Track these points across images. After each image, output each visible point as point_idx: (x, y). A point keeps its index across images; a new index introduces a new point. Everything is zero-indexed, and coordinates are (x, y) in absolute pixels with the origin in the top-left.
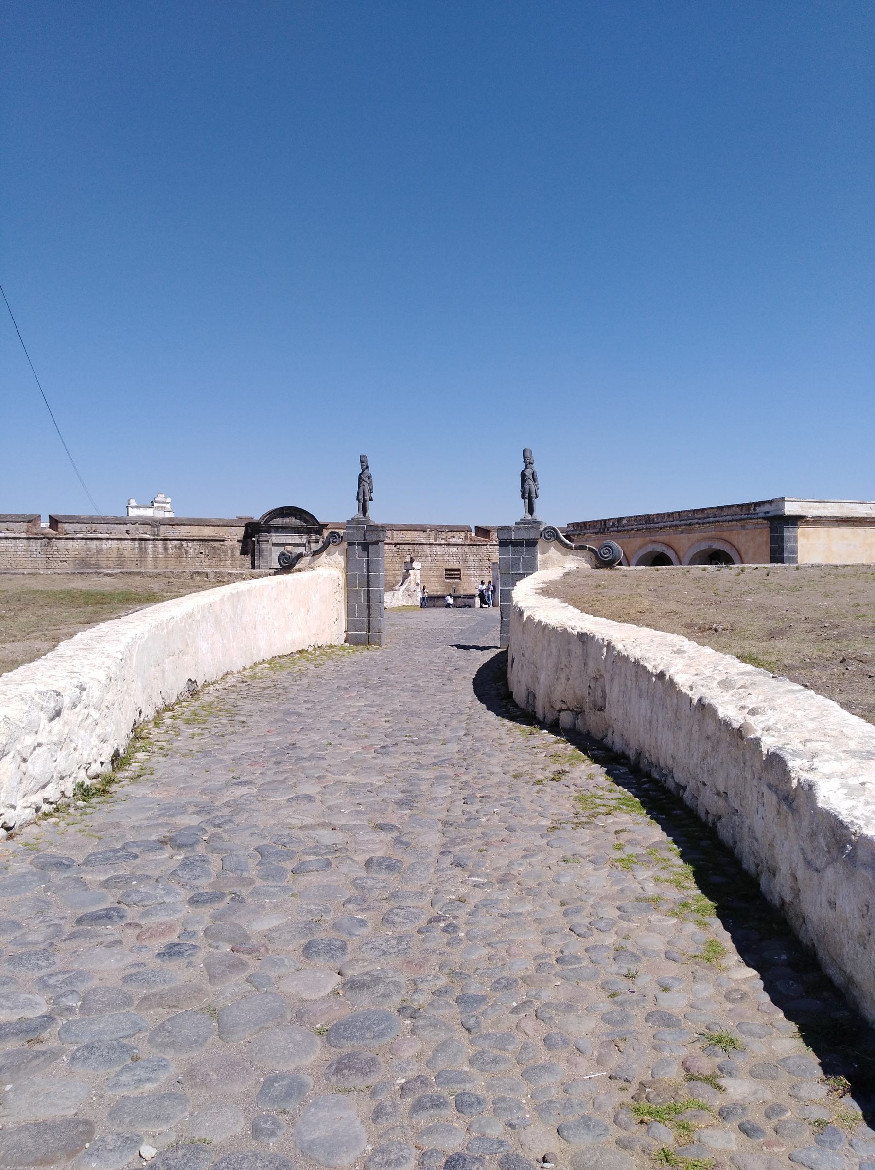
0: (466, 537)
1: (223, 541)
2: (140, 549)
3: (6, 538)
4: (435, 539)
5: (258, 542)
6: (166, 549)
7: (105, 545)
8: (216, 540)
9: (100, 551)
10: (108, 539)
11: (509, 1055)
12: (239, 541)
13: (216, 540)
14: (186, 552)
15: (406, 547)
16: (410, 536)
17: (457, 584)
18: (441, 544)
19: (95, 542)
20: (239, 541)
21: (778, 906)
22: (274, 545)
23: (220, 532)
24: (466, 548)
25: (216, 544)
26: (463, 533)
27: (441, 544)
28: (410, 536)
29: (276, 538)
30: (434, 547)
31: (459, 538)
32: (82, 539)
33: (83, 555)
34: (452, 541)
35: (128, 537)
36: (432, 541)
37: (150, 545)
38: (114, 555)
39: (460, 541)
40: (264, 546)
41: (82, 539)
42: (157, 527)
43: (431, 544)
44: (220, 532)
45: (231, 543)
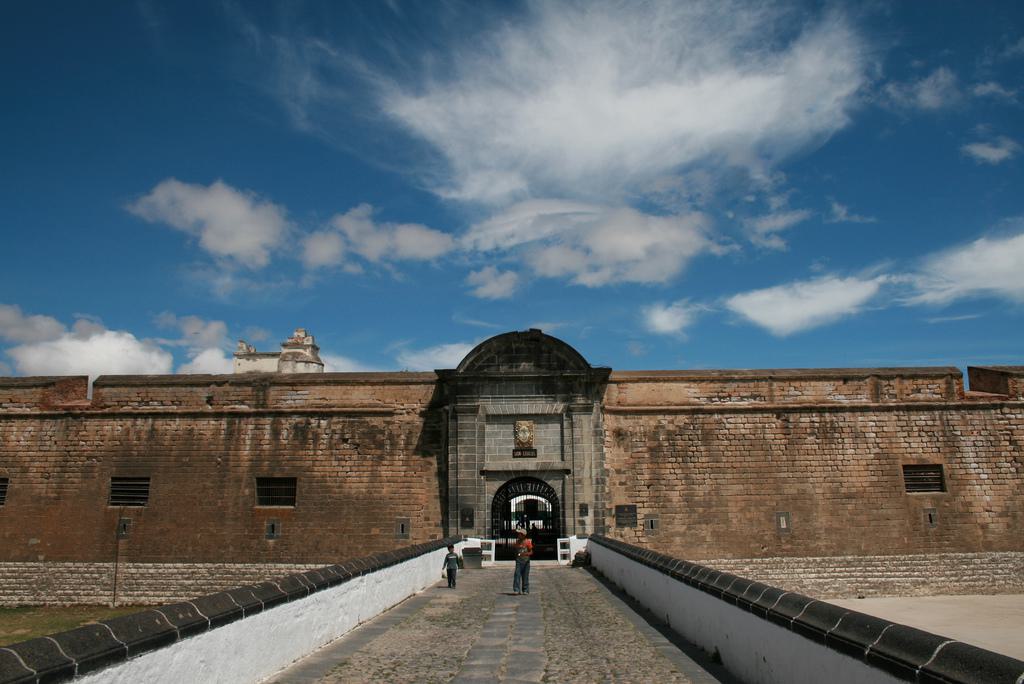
0: (949, 392)
1: (390, 414)
5: (455, 411)
6: (276, 433)
8: (376, 414)
11: (678, 548)
13: (376, 414)
21: (419, 112)
22: (494, 419)
23: (387, 397)
25: (376, 421)
28: (811, 393)
29: (89, 404)
31: (930, 392)
37: (249, 427)
40: (463, 421)
44: (387, 397)
45: (407, 418)
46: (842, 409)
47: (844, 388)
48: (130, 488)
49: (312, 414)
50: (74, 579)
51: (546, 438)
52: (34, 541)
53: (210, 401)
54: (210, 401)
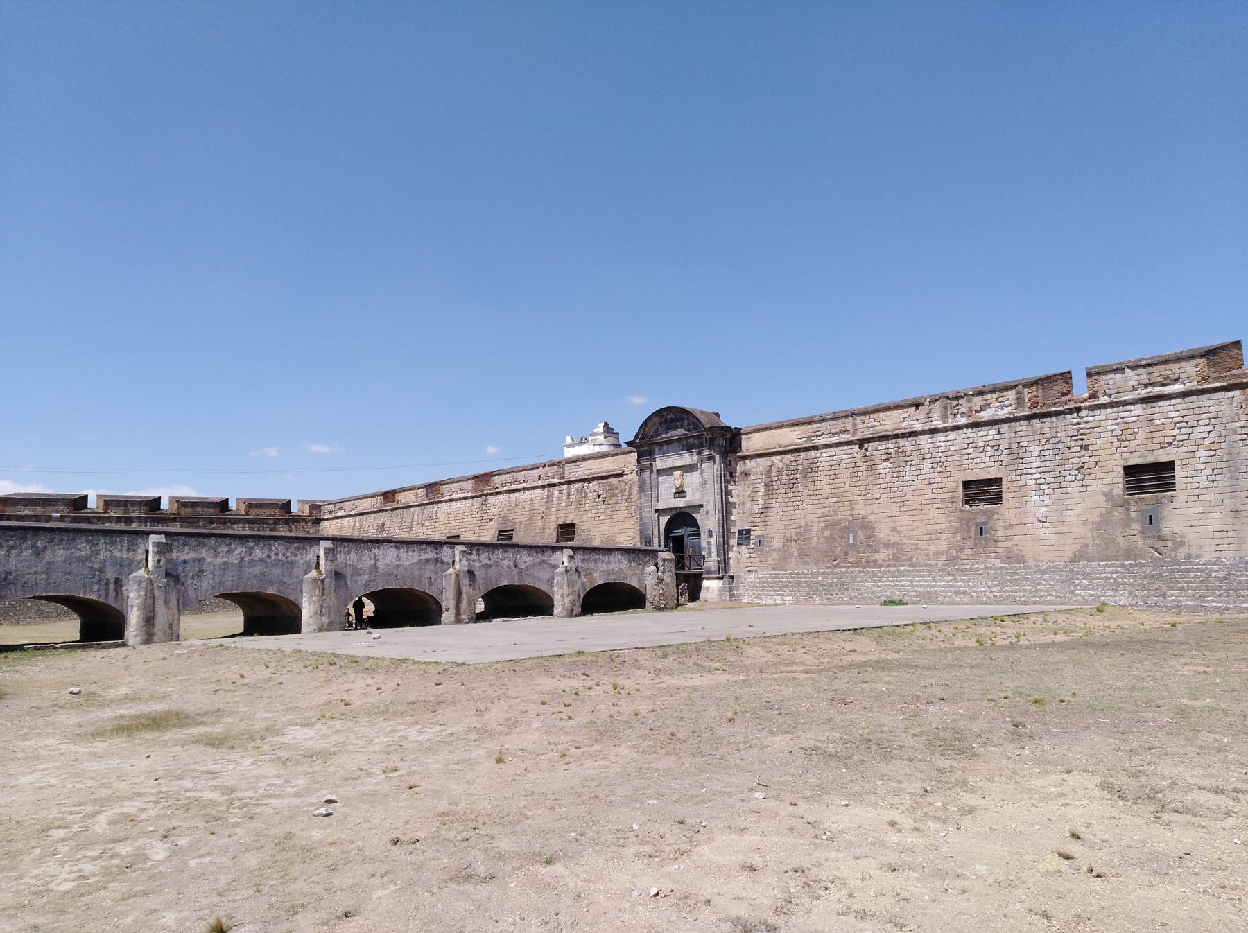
0: (1020, 402)
3: (460, 499)
4: (944, 418)
7: (522, 496)
10: (525, 489)
15: (882, 446)
18: (956, 428)
24: (1022, 427)
25: (614, 481)
26: (1012, 394)
27: (956, 428)
28: (889, 422)
30: (941, 437)
32: (507, 492)
34: (985, 415)
35: (540, 483)
36: (938, 424)
38: (527, 507)
39: (1004, 413)
41: (507, 492)
43: (934, 431)
46: (913, 434)
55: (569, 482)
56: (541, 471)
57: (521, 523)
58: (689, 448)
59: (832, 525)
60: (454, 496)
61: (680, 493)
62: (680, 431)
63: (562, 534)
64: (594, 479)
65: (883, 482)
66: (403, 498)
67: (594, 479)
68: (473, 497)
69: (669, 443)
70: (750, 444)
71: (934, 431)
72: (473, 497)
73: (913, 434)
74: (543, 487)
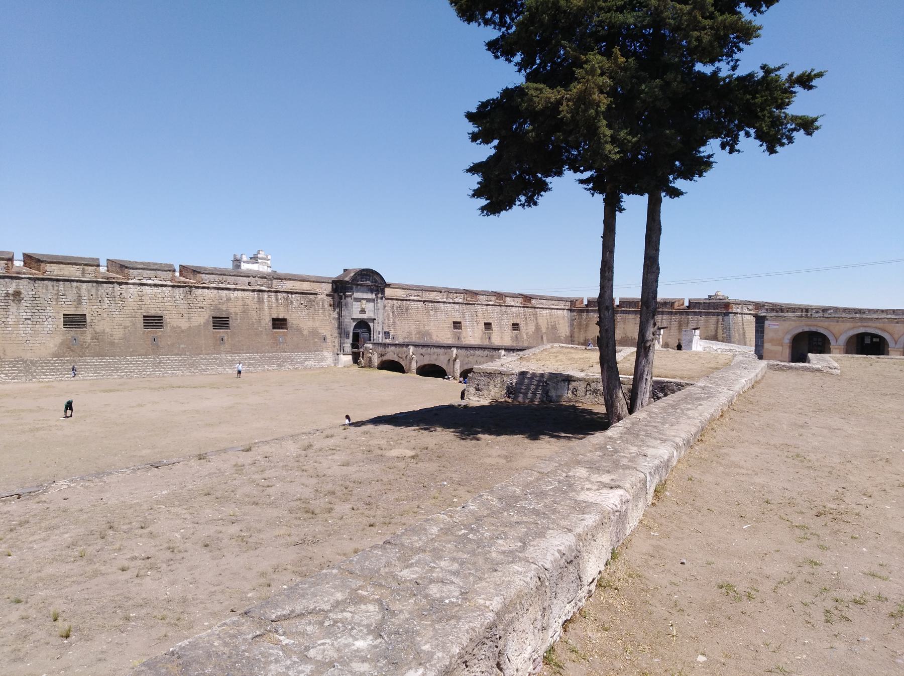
2: (259, 299)
7: (233, 294)
9: (229, 299)
10: (235, 289)
12: (327, 295)
14: (292, 303)
15: (430, 304)
16: (433, 296)
17: (460, 333)
19: (225, 292)
20: (327, 295)
23: (315, 287)
25: (311, 297)
28: (433, 296)
33: (216, 302)
34: (456, 300)
36: (445, 300)
38: (240, 303)
39: (460, 301)
40: (349, 300)
42: (271, 280)
43: (444, 302)
46: (439, 302)
47: (440, 295)
48: (220, 322)
49: (291, 293)
50: (204, 362)
51: (369, 306)
52: (182, 346)
53: (249, 284)
54: (249, 284)
55: (276, 292)
56: (251, 279)
57: (237, 314)
58: (372, 291)
59: (419, 333)
60: (144, 281)
61: (363, 311)
62: (369, 283)
63: (273, 324)
64: (296, 293)
65: (432, 318)
66: (509, 301)
67: (296, 293)
68: (173, 286)
69: (361, 285)
70: (388, 292)
71: (444, 302)
72: (173, 286)
73: (439, 302)
74: (253, 291)
